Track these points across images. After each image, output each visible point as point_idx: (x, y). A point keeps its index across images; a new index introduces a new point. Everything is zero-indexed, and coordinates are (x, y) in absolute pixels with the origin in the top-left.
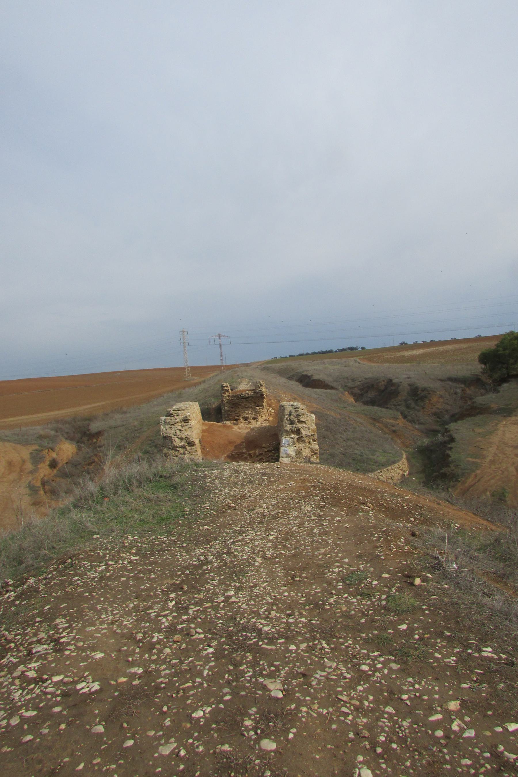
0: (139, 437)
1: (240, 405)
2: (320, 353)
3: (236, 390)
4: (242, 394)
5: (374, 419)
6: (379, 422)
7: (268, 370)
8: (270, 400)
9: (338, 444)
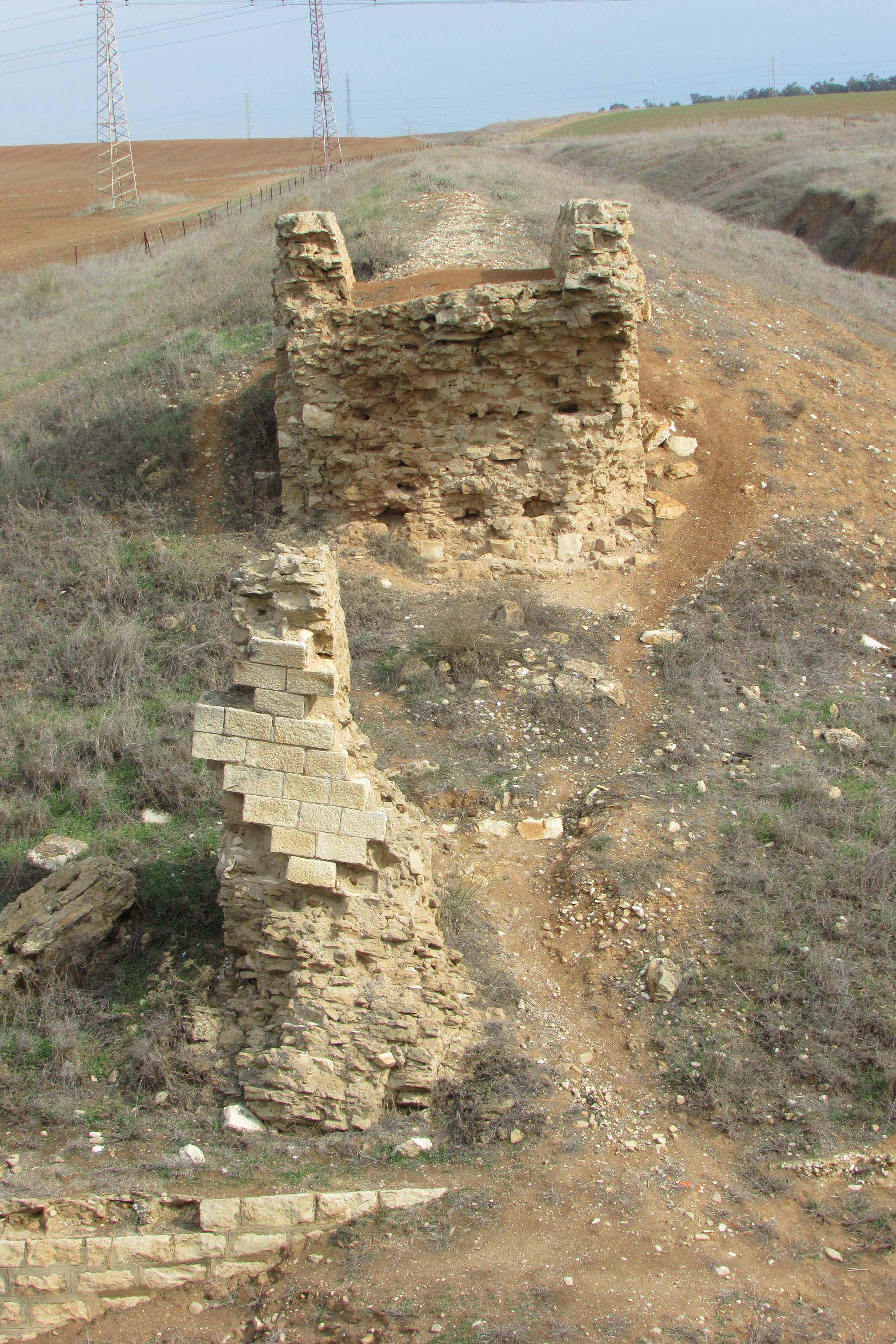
1: (429, 395)
2: (856, 87)
3: (396, 272)
4: (444, 305)
7: (588, 163)
8: (663, 353)
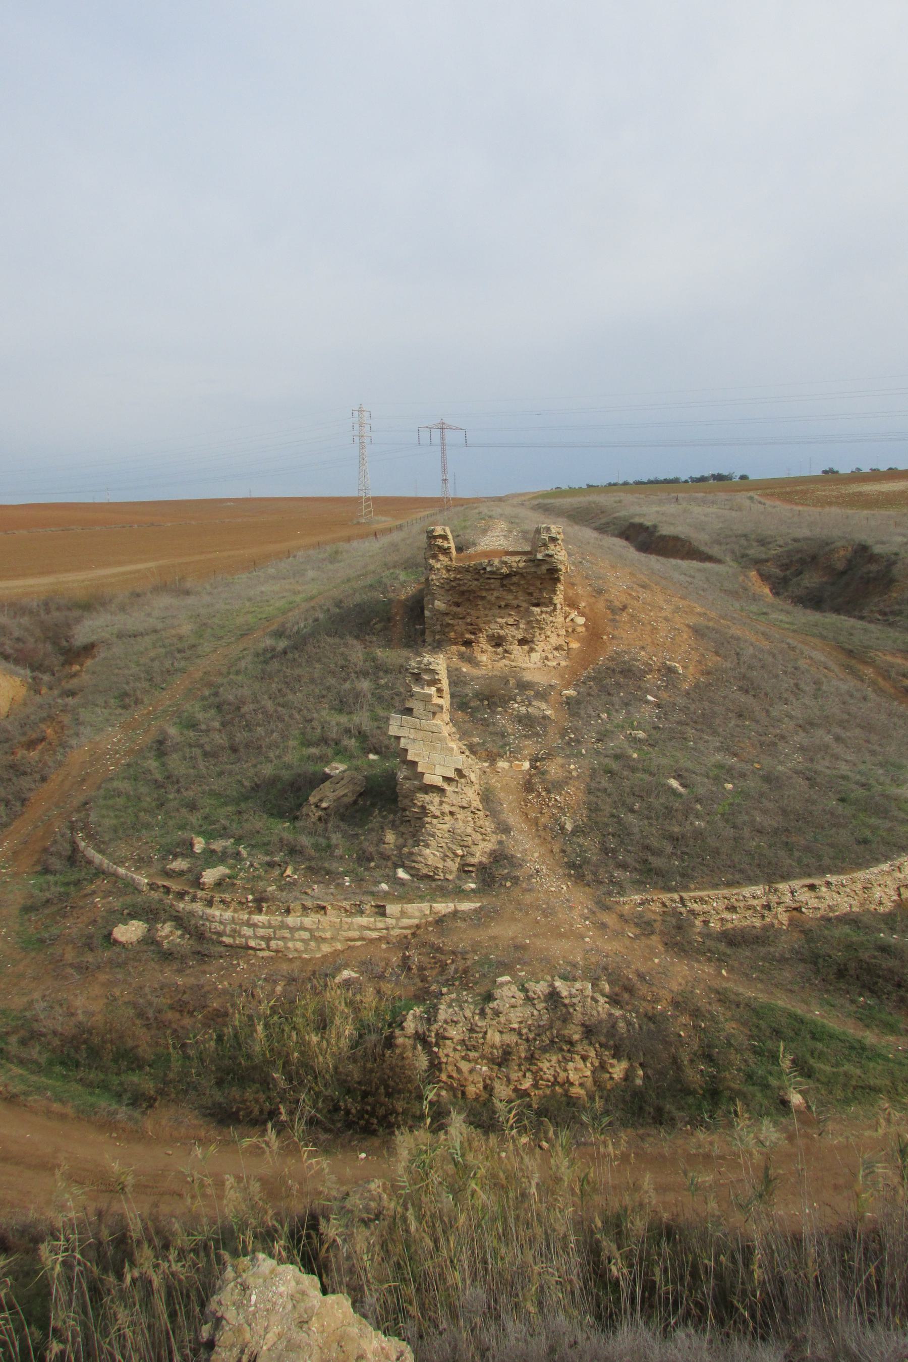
0: (183, 671)
1: (483, 598)
2: (650, 482)
3: (471, 551)
5: (850, 653)
6: (865, 663)
8: (573, 585)
9: (783, 737)
